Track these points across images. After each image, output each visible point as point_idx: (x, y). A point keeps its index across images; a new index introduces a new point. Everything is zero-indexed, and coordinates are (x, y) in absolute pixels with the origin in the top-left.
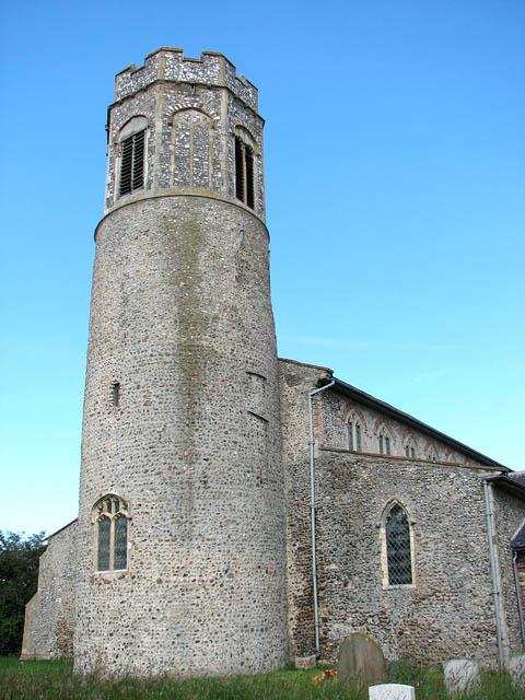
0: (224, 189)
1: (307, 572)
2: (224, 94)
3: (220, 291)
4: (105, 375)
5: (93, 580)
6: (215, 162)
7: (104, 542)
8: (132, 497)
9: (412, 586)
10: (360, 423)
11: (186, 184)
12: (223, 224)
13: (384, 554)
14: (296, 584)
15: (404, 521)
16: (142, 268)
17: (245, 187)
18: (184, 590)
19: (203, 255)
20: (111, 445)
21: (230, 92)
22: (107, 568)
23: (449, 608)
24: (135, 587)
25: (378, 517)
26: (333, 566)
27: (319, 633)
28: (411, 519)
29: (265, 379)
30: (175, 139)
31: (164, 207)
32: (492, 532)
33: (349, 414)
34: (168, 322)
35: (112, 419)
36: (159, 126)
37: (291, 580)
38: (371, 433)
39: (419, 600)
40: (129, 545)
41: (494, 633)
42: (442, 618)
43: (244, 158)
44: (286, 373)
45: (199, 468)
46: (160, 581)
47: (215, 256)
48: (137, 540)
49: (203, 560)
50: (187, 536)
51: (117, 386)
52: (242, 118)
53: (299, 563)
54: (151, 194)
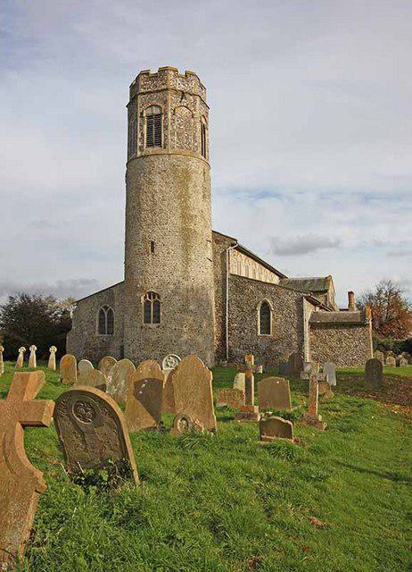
39: (272, 341)
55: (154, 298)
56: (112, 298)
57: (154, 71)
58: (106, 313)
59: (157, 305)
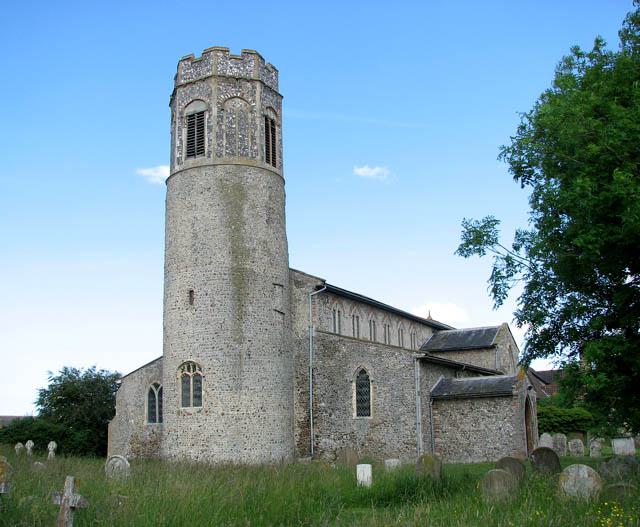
0: (259, 158)
1: (306, 407)
2: (258, 85)
3: (256, 230)
4: (183, 281)
5: (179, 413)
6: (253, 138)
7: (186, 390)
8: (205, 363)
9: (371, 418)
10: (341, 310)
11: (234, 154)
12: (256, 181)
13: (354, 398)
14: (300, 414)
15: (367, 378)
16: (206, 214)
17: (272, 154)
18: (238, 419)
19: (246, 207)
20: (189, 330)
21: (261, 82)
22: (188, 405)
23: (391, 431)
24: (208, 418)
25: (352, 375)
26: (323, 404)
27: (313, 444)
28: (371, 378)
29: (282, 286)
30: (226, 121)
31: (220, 172)
32: (418, 389)
33: (334, 305)
34: (225, 253)
35: (189, 313)
36: (215, 111)
37: (296, 412)
38: (346, 315)
39: (374, 426)
40: (203, 392)
41: (416, 446)
42: (385, 435)
43: (271, 127)
44: (296, 279)
45: (246, 346)
46: (223, 414)
47: (253, 207)
48: (209, 390)
49: (248, 401)
50: (239, 388)
51: (191, 292)
52: (270, 100)
53: (301, 402)
54: (210, 161)
55: (194, 370)
56: (160, 368)
57: (198, 56)
58: (156, 393)
59: (198, 380)
